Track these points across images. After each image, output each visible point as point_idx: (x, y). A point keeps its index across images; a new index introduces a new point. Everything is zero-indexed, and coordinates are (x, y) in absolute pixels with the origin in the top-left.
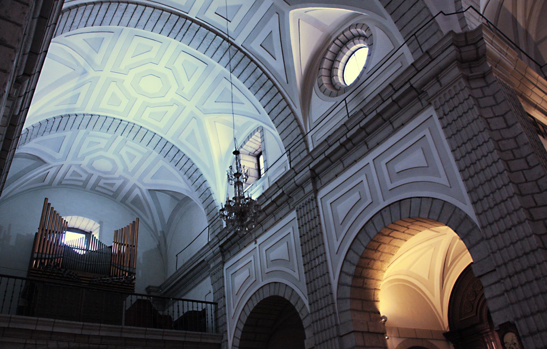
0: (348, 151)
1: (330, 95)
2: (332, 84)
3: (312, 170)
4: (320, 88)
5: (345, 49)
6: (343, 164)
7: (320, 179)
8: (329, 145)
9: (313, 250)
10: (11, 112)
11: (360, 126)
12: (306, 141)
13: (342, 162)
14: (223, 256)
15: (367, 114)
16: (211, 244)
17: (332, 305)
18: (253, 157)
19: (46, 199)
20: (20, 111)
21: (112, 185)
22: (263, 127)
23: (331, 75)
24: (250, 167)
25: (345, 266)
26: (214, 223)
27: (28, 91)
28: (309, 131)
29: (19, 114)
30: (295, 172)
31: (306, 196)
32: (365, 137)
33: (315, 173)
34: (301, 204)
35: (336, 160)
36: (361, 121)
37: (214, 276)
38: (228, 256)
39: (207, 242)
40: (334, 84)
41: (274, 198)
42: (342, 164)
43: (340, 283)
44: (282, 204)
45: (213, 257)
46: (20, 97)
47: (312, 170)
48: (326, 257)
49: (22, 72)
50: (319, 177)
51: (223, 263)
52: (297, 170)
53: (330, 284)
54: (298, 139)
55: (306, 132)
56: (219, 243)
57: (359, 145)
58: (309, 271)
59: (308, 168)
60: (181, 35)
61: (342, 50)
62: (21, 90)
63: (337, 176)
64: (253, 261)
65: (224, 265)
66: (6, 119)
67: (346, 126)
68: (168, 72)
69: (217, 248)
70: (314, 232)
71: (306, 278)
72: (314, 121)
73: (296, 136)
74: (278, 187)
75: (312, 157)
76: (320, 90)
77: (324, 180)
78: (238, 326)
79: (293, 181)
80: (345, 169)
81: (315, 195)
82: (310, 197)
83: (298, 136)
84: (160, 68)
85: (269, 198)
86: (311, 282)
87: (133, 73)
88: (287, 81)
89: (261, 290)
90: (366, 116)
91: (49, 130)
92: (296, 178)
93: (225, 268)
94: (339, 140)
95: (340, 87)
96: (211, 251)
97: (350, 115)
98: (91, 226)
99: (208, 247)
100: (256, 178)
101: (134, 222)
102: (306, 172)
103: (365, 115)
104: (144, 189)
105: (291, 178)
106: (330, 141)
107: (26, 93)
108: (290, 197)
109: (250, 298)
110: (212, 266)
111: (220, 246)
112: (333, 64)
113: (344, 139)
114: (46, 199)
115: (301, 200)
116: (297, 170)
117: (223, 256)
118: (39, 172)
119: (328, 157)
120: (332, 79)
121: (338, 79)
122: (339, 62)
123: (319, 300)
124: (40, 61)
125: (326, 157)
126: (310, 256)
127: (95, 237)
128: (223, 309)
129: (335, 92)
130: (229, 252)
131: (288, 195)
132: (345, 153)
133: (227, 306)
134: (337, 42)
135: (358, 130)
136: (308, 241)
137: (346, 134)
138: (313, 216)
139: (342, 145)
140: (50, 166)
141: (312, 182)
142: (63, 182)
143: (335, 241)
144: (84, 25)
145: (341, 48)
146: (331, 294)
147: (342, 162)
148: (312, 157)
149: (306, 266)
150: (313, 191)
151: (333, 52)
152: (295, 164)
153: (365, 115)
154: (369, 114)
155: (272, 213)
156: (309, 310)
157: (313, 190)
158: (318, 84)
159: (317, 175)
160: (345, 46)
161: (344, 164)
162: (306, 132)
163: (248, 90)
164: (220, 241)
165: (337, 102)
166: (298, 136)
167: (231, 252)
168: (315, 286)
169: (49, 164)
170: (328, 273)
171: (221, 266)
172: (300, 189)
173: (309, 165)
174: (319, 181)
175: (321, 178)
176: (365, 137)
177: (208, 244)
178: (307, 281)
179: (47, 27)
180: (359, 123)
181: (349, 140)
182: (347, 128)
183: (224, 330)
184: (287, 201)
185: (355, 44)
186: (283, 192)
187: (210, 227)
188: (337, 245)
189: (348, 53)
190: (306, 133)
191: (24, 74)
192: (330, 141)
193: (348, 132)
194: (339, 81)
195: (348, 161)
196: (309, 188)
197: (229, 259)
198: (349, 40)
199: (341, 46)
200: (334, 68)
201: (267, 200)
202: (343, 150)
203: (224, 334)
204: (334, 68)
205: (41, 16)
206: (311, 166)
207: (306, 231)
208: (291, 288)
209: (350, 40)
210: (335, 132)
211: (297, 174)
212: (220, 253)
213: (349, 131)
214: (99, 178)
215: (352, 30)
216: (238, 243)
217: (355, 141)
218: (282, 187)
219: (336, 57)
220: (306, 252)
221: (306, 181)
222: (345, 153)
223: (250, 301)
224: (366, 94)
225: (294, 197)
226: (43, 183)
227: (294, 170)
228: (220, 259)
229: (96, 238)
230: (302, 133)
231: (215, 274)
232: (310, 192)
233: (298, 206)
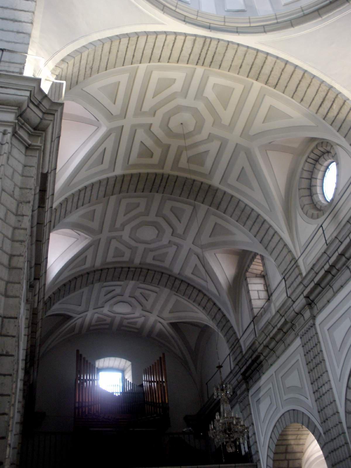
0: (334, 276)
1: (312, 217)
2: (314, 205)
3: (307, 297)
4: (302, 209)
5: (318, 166)
6: (333, 289)
7: (316, 304)
8: (316, 273)
9: (319, 378)
10: (31, 306)
11: (338, 253)
12: (298, 266)
13: (331, 287)
14: (247, 383)
15: (342, 241)
16: (234, 372)
17: (343, 435)
18: (260, 278)
19: (78, 351)
20: (38, 302)
21: (135, 323)
22: (217, 326)
23: (311, 194)
24: (259, 290)
25: (348, 393)
26: (234, 350)
27: (40, 287)
28: (299, 254)
29: (38, 305)
30: (292, 300)
31: (306, 322)
32: (346, 262)
33: (310, 299)
34: (303, 330)
35: (326, 286)
36: (338, 248)
37: (241, 404)
38: (251, 382)
39: (230, 371)
40: (315, 204)
41: (279, 326)
42: (331, 289)
43: (347, 411)
44: (288, 331)
45: (238, 385)
46: (35, 295)
47: (307, 297)
48: (330, 385)
49: (32, 279)
50: (314, 303)
51: (248, 390)
52: (293, 297)
53: (338, 412)
54: (291, 265)
55: (298, 256)
56: (240, 371)
57: (342, 269)
58: (318, 399)
59: (302, 297)
60: (161, 189)
61: (316, 167)
62: (35, 290)
63: (329, 302)
64: (272, 388)
65: (248, 392)
66: (29, 312)
67: (327, 254)
68: (160, 220)
69: (239, 377)
70: (317, 360)
71: (318, 406)
72: (302, 246)
73: (289, 262)
74: (281, 315)
75: (304, 286)
76: (303, 211)
77: (320, 305)
78: (268, 454)
79: (292, 309)
80: (336, 293)
81: (313, 321)
82: (309, 324)
83: (291, 262)
84: (152, 217)
85: (262, 344)
86: (322, 410)
87: (128, 228)
88: (263, 445)
89: (283, 417)
90: (342, 243)
91: (68, 291)
92: (294, 306)
93: (250, 395)
94: (323, 267)
95: (321, 207)
96: (235, 379)
97: (328, 242)
98: (124, 365)
99: (231, 375)
100: (266, 300)
101: (160, 358)
102: (301, 301)
103: (340, 242)
104: (165, 323)
105: (290, 306)
106: (316, 269)
107: (39, 290)
108: (293, 324)
109: (275, 426)
110: (238, 393)
111: (242, 374)
112: (311, 181)
113: (327, 267)
114: (78, 351)
115: (303, 327)
116: (293, 297)
117: (247, 383)
118: (69, 325)
119: (318, 284)
120: (313, 198)
121: (318, 197)
122: (316, 179)
123: (331, 429)
124: (52, 181)
125: (315, 284)
126: (317, 384)
127: (128, 381)
128: (253, 437)
129: (315, 212)
130: (251, 378)
131: (291, 323)
132: (332, 279)
133: (256, 434)
134: (310, 160)
135: (337, 257)
136: (314, 368)
137: (328, 261)
138: (314, 343)
139: (328, 272)
140: (75, 319)
141: (309, 308)
142: (91, 328)
143: (336, 367)
144: (75, 208)
145: (315, 165)
146: (341, 423)
147: (331, 287)
148: (304, 286)
149: (316, 394)
150: (311, 318)
151: (308, 171)
152: (291, 292)
153: (340, 242)
154: (344, 240)
155: (281, 339)
156: (324, 438)
157: (310, 317)
158: (301, 205)
159: (313, 301)
160: (317, 163)
161: (334, 289)
162: (298, 256)
163: (236, 222)
164: (241, 369)
165: (318, 224)
166: (291, 262)
167: (253, 379)
168: (325, 414)
169: (75, 317)
170: (335, 401)
171: (246, 393)
172: (299, 316)
173: (302, 293)
174: (316, 306)
175: (317, 303)
176: (346, 262)
177: (231, 372)
178: (318, 409)
179: (43, 244)
180: (337, 250)
181: (333, 266)
182: (328, 256)
183: (257, 459)
184: (291, 327)
185: (326, 160)
186: (286, 320)
187: (231, 355)
188: (338, 371)
189: (323, 169)
190: (297, 258)
191: (35, 279)
192: (316, 269)
193: (329, 259)
194: (319, 199)
195: (336, 286)
196: (307, 314)
197: (252, 386)
198: (312, 172)
199: (314, 163)
200: (313, 186)
201: (274, 328)
202: (329, 277)
203: (258, 463)
204: (313, 186)
205: (37, 241)
206: (305, 293)
207: (318, 351)
208: (307, 416)
209: (321, 156)
210: (318, 260)
211: (294, 302)
212: (243, 381)
213: (330, 258)
214: (122, 319)
215: (320, 148)
216: (257, 370)
217: (338, 266)
218: (284, 316)
219: (312, 174)
220: (313, 379)
221: (303, 308)
222: (332, 279)
223: (275, 428)
224: (342, 215)
225: (297, 324)
226: (102, 165)
227: (291, 298)
228: (244, 386)
229: (130, 381)
230: (294, 258)
231: (242, 401)
232: (308, 320)
233: (300, 333)
